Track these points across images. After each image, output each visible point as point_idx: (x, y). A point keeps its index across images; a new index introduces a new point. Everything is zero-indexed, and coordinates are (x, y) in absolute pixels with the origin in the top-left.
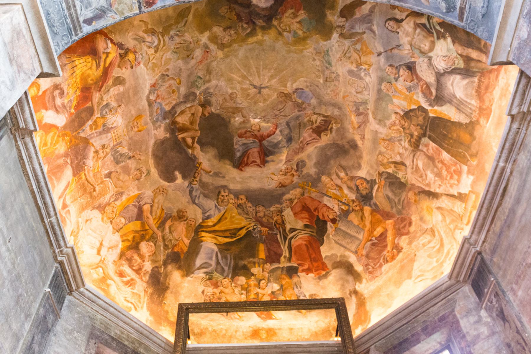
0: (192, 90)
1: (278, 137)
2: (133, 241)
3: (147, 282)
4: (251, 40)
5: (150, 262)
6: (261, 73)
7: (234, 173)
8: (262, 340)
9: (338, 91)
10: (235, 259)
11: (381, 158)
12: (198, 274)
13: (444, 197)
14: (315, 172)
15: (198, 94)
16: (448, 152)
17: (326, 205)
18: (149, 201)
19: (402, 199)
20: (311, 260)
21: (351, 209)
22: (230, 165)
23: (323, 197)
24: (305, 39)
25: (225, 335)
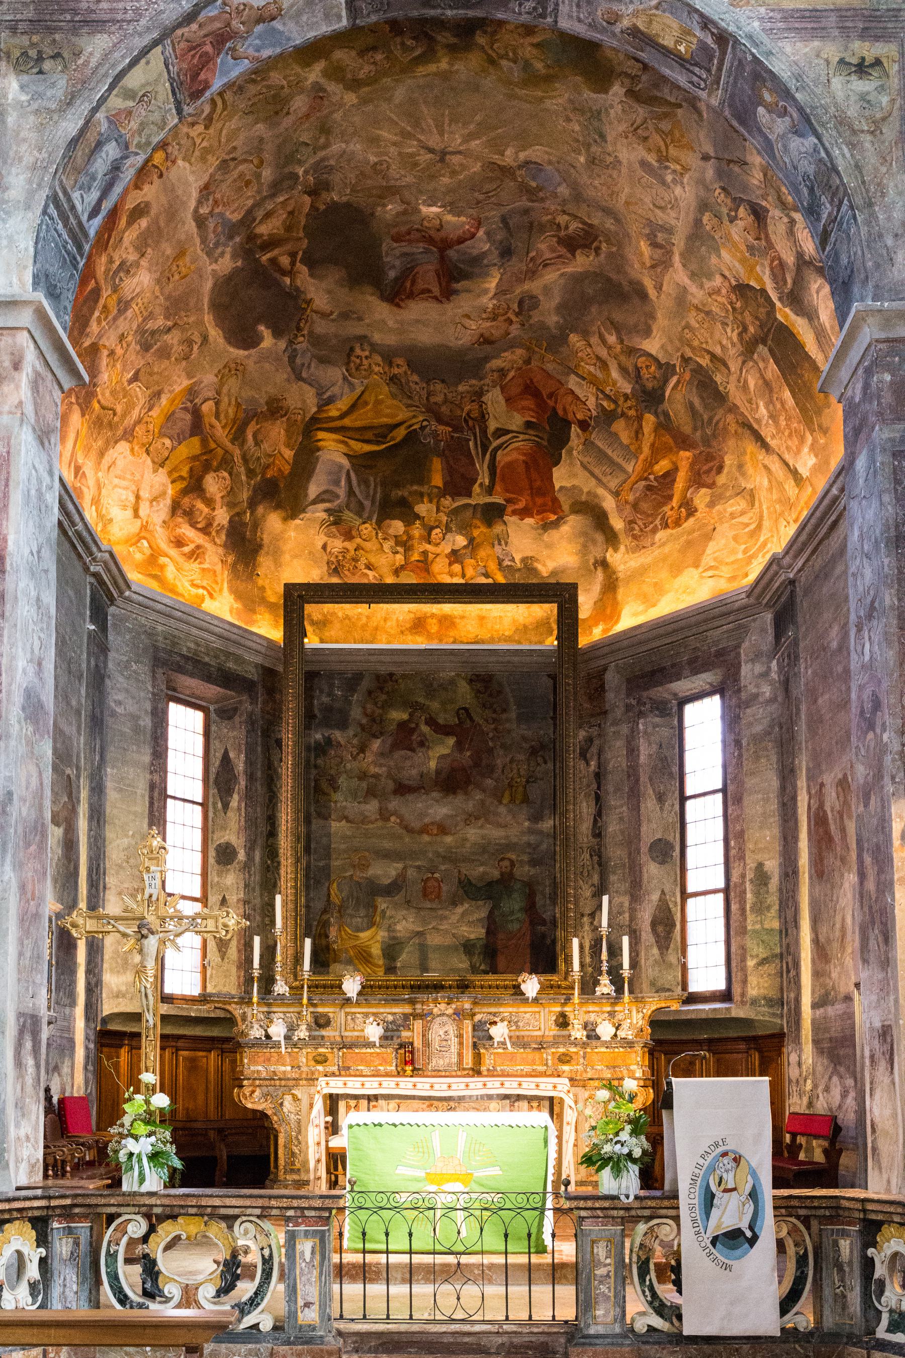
0: (286, 170)
1: (482, 244)
2: (191, 477)
3: (225, 546)
4: (421, 70)
5: (225, 508)
6: (446, 128)
7: (381, 311)
8: (430, 637)
9: (616, 189)
10: (384, 484)
11: (688, 335)
12: (314, 512)
13: (776, 458)
14: (557, 322)
15: (301, 173)
16: (792, 392)
17: (572, 392)
18: (211, 394)
19: (717, 418)
20: (532, 493)
21: (619, 410)
22: (372, 294)
23: (568, 374)
24: (548, 79)
25: (366, 625)
